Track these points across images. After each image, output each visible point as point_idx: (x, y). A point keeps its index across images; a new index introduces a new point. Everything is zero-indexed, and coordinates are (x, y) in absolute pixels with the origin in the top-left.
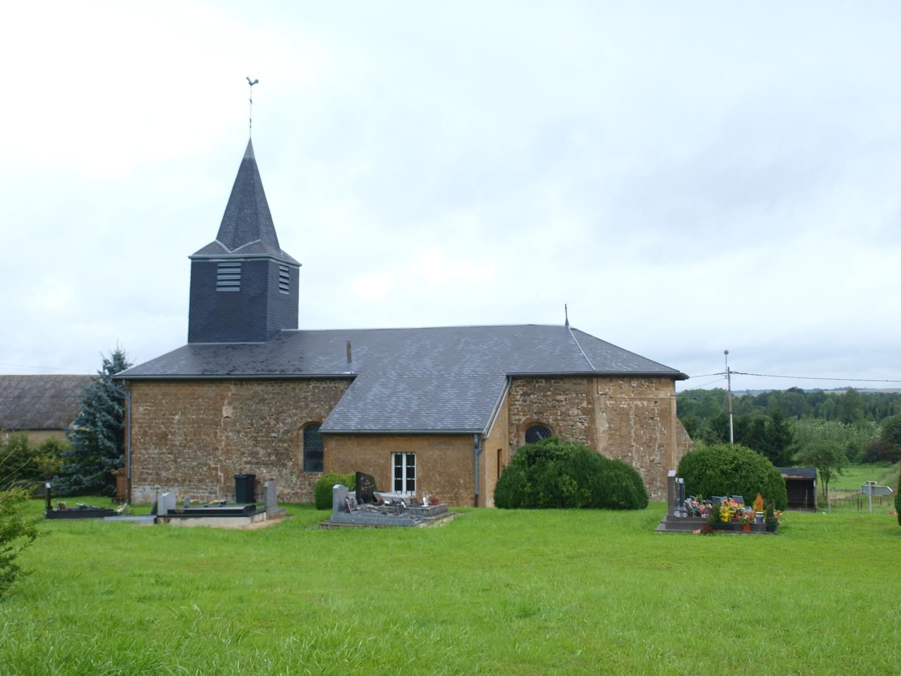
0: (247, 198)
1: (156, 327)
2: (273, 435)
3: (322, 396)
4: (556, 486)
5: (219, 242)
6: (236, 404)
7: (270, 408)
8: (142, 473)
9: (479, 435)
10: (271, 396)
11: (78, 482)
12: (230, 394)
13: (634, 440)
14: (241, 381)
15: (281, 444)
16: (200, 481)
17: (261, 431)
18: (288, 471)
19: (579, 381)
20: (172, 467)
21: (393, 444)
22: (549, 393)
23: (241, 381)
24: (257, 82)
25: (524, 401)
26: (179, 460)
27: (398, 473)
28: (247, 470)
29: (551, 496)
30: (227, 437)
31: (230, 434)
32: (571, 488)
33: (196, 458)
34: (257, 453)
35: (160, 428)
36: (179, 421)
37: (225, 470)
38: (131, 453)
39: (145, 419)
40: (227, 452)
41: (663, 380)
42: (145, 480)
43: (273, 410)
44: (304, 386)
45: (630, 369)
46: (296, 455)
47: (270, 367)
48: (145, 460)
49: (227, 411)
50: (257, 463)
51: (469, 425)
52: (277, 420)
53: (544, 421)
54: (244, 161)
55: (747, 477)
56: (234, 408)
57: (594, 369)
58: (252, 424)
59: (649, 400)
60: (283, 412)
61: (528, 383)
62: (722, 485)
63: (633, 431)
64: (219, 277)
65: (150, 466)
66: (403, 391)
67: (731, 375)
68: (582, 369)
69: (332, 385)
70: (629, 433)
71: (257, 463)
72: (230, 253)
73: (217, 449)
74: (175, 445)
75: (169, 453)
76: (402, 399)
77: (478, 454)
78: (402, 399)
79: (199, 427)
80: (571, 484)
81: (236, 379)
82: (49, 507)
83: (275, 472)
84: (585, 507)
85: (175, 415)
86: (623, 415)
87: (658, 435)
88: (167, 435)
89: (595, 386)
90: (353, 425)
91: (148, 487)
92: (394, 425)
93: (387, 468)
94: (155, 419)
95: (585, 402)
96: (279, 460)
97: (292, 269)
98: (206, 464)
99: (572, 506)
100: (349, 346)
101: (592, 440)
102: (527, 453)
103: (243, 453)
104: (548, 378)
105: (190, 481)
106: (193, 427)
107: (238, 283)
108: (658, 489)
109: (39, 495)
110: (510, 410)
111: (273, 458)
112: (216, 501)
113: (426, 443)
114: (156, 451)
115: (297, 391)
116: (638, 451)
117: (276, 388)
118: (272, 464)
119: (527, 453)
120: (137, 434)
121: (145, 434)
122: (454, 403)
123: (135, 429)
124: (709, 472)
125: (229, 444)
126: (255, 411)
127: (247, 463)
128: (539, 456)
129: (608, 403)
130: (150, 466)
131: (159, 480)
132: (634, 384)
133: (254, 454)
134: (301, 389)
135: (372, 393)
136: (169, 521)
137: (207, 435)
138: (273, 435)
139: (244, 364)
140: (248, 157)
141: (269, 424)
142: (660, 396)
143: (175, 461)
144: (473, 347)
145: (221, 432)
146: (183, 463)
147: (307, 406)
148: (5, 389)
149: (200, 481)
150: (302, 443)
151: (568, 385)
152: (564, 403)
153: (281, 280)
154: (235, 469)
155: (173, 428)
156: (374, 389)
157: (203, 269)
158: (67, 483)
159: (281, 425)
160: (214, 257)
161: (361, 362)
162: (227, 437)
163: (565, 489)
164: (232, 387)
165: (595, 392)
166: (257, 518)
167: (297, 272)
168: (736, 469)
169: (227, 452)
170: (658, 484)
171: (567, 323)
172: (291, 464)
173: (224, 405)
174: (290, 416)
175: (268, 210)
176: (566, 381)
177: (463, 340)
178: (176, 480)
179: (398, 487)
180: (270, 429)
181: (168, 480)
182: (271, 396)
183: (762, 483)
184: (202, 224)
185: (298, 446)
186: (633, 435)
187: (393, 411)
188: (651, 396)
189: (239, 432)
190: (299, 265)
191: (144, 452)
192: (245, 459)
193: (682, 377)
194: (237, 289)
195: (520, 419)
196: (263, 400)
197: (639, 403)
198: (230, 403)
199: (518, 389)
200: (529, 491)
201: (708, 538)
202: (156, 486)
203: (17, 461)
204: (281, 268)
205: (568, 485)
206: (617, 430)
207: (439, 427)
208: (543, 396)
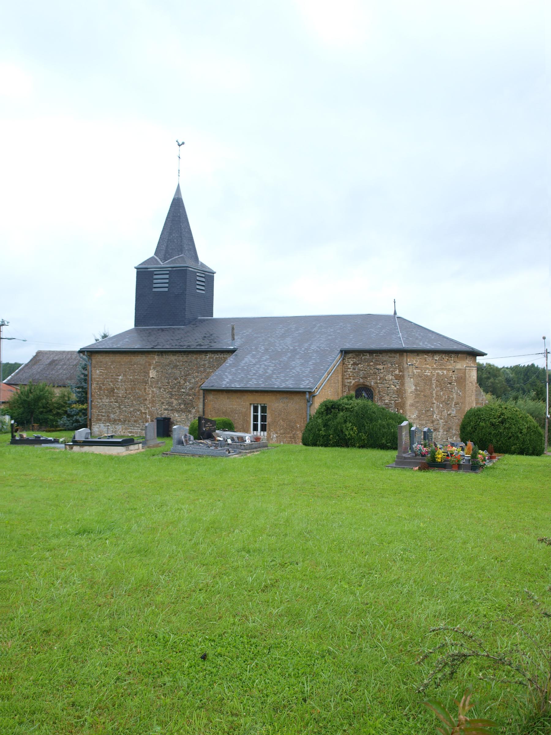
0: (177, 227)
1: (115, 315)
2: (183, 390)
3: (215, 364)
4: (342, 431)
5: (156, 257)
6: (159, 369)
7: (181, 371)
8: (98, 415)
9: (310, 392)
10: (181, 363)
11: (77, 421)
12: (154, 362)
13: (435, 399)
14: (162, 353)
15: (187, 397)
16: (135, 421)
17: (175, 388)
18: (192, 416)
19: (393, 355)
20: (117, 411)
21: (251, 398)
22: (372, 363)
23: (162, 353)
24: (183, 143)
25: (354, 369)
26: (122, 407)
27: (255, 418)
28: (165, 414)
29: (337, 437)
30: (153, 391)
31: (155, 389)
32: (351, 433)
33: (133, 405)
34: (172, 403)
35: (110, 384)
36: (121, 380)
37: (151, 414)
38: (91, 401)
39: (100, 378)
40: (153, 402)
41: (460, 355)
42: (100, 420)
43: (183, 373)
44: (203, 356)
45: (433, 347)
46: (197, 405)
47: (181, 344)
48: (100, 407)
49: (152, 374)
50: (172, 410)
51: (303, 385)
52: (185, 380)
53: (368, 384)
54: (174, 199)
55: (510, 428)
56: (157, 372)
57: (404, 346)
58: (168, 383)
59: (448, 370)
60: (189, 375)
61: (357, 356)
62: (490, 433)
63: (434, 392)
64: (155, 281)
65: (104, 411)
66: (265, 361)
67: (548, 354)
68: (395, 346)
69: (222, 356)
70: (432, 393)
71: (172, 410)
72: (162, 264)
73: (146, 399)
74: (119, 397)
75: (115, 402)
76: (263, 366)
77: (310, 407)
78: (263, 366)
79: (135, 384)
80: (352, 429)
81: (158, 352)
82: (13, 437)
83: (184, 416)
84: (362, 446)
85: (119, 376)
86: (427, 380)
87: (455, 396)
88: (114, 390)
89: (405, 359)
90: (224, 384)
91: (102, 425)
92: (252, 384)
93: (247, 415)
94: (106, 378)
95: (398, 370)
96: (186, 408)
97: (208, 277)
98: (139, 410)
99: (353, 446)
100: (233, 329)
101: (402, 398)
102: (326, 406)
103: (163, 403)
104: (371, 352)
105: (129, 421)
106: (130, 385)
107: (167, 285)
108: (454, 435)
109: (59, 429)
110: (343, 375)
111: (182, 406)
112: (106, 435)
113: (274, 398)
114: (107, 401)
115: (199, 360)
116: (438, 407)
117: (181, 358)
118: (182, 411)
119: (326, 406)
120: (95, 389)
121: (100, 388)
122: (298, 369)
123: (94, 385)
124: (482, 424)
125: (154, 397)
126: (170, 373)
127: (165, 409)
128: (334, 408)
129: (415, 371)
130: (104, 411)
131: (109, 420)
132: (437, 357)
133: (170, 404)
134: (201, 359)
135: (244, 362)
136: (72, 448)
137: (139, 390)
138: (183, 390)
139: (165, 341)
140: (177, 197)
141: (180, 383)
142: (457, 367)
143: (119, 407)
144: (323, 330)
145: (149, 388)
146: (124, 409)
147: (205, 370)
148: (68, 360)
149: (135, 421)
150: (202, 397)
151: (385, 358)
152: (382, 371)
153: (198, 283)
154: (158, 414)
155: (118, 385)
156: (246, 360)
157: (144, 275)
158: (71, 421)
159: (188, 384)
160: (152, 267)
161: (243, 340)
162: (153, 391)
163: (347, 433)
164: (156, 357)
165: (405, 363)
166: (132, 447)
167: (212, 278)
168: (502, 422)
169: (153, 402)
170: (454, 432)
171: (395, 313)
172: (194, 410)
173: (150, 369)
174: (194, 378)
175: (191, 234)
176: (384, 354)
177: (318, 325)
178: (120, 420)
179: (255, 429)
180: (180, 387)
181: (115, 420)
182: (181, 363)
183: (521, 433)
184: (145, 245)
185: (199, 398)
186: (434, 395)
187: (255, 374)
188: (450, 367)
189: (160, 388)
190: (214, 273)
191: (100, 401)
192: (164, 407)
193: (482, 354)
194: (166, 289)
195: (351, 382)
196: (176, 366)
197: (440, 372)
198: (154, 368)
199: (350, 360)
200: (324, 433)
201: (421, 474)
202: (107, 424)
203: (64, 406)
204: (198, 274)
205: (350, 430)
206: (422, 392)
207: (283, 386)
208: (368, 366)
